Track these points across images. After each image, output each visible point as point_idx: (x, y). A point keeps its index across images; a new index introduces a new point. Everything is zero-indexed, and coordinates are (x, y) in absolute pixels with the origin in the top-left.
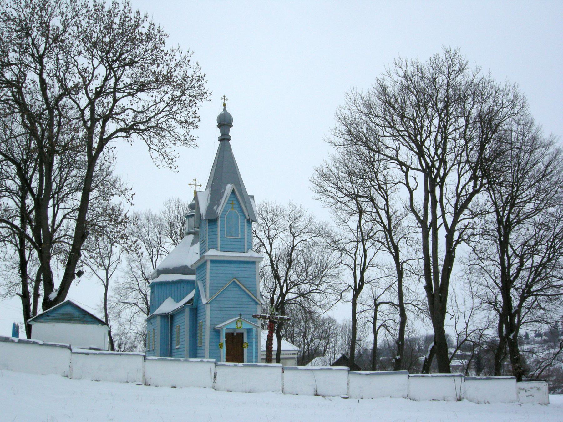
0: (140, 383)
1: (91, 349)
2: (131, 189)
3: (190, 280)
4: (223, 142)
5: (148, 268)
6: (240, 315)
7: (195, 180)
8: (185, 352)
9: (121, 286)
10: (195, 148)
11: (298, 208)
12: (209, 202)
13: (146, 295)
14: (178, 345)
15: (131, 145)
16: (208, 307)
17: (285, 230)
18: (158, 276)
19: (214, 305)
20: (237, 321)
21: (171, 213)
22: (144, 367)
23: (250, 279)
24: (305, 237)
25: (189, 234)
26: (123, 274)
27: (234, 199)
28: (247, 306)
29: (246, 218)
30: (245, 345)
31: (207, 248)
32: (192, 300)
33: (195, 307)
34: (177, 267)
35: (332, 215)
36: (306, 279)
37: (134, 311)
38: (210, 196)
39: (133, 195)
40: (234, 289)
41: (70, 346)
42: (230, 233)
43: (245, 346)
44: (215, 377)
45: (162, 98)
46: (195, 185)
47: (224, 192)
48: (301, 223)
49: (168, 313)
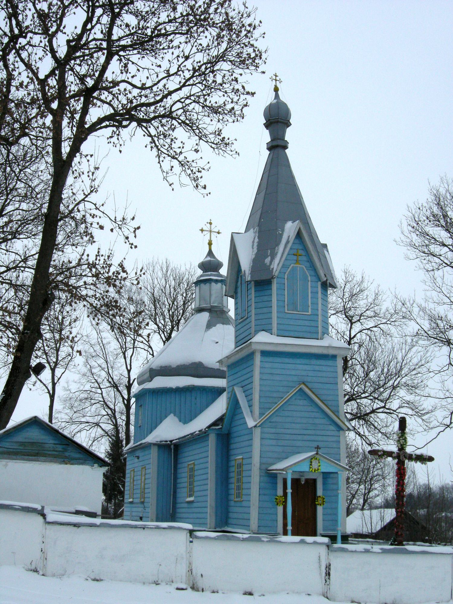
0: (184, 586)
1: (78, 512)
2: (133, 219)
3: (207, 387)
4: (276, 151)
5: (118, 369)
6: (318, 448)
7: (211, 223)
8: (209, 510)
9: (74, 396)
10: (234, 156)
11: (358, 278)
12: (255, 250)
13: (114, 411)
14: (190, 496)
15: (120, 151)
16: (257, 433)
17: (337, 312)
18: (151, 379)
19: (266, 430)
20: (311, 458)
21: (156, 282)
22: (189, 553)
23: (328, 386)
24: (370, 324)
25: (200, 310)
26: (77, 377)
27: (300, 247)
28: (323, 433)
29: (319, 279)
30: (320, 501)
31: (253, 330)
32: (220, 420)
33: (226, 432)
34: (184, 365)
35: (428, 288)
36: (364, 392)
37: (93, 435)
38: (257, 240)
39: (135, 229)
40: (301, 402)
41: (43, 508)
42: (293, 306)
43: (320, 502)
44: (328, 574)
45: (179, 66)
46: (211, 231)
47: (281, 235)
48: (362, 303)
49: (171, 441)
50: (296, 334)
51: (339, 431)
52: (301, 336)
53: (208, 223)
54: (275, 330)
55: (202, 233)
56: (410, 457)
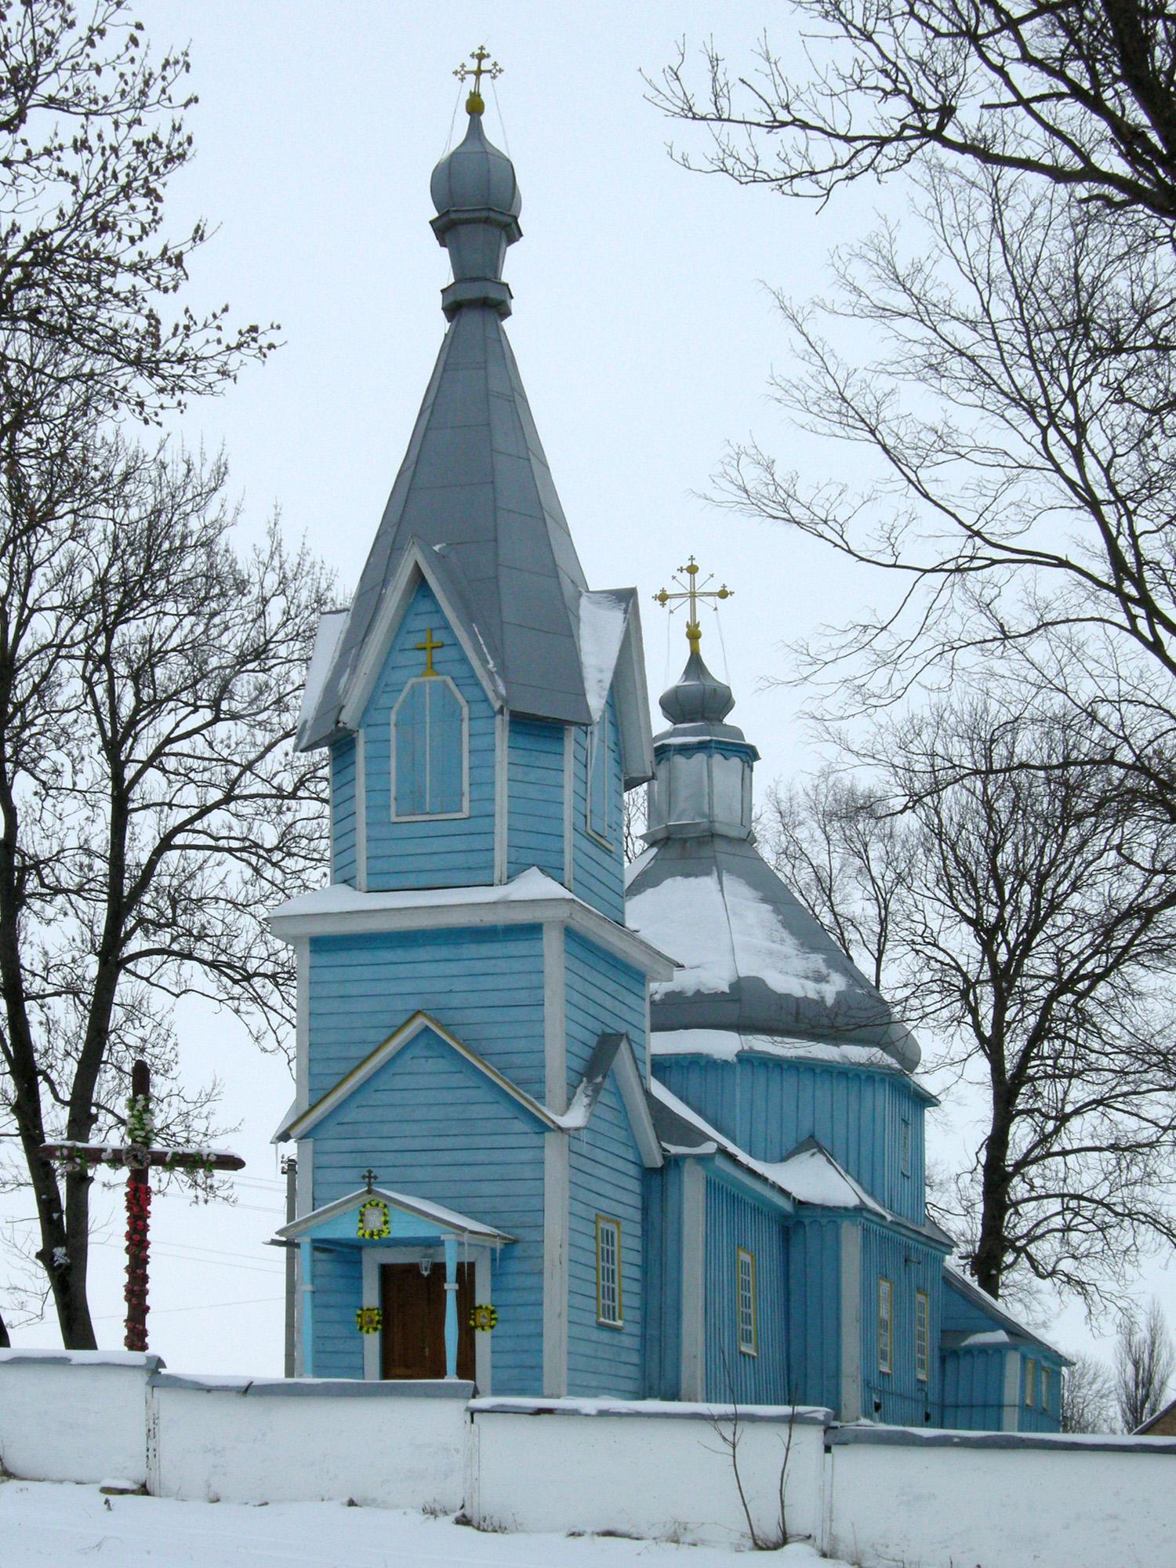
4: (472, 318)
19: (331, 1145)
23: (514, 1013)
28: (499, 1141)
40: (431, 1065)
42: (413, 800)
43: (481, 1320)
46: (693, 595)
50: (424, 880)
51: (543, 1133)
52: (393, 885)
53: (681, 570)
54: (362, 878)
55: (663, 605)
56: (159, 1159)
